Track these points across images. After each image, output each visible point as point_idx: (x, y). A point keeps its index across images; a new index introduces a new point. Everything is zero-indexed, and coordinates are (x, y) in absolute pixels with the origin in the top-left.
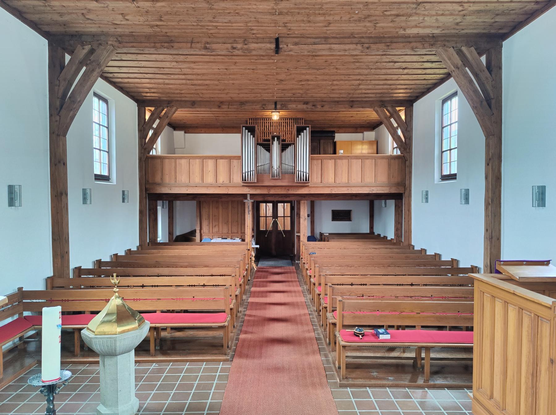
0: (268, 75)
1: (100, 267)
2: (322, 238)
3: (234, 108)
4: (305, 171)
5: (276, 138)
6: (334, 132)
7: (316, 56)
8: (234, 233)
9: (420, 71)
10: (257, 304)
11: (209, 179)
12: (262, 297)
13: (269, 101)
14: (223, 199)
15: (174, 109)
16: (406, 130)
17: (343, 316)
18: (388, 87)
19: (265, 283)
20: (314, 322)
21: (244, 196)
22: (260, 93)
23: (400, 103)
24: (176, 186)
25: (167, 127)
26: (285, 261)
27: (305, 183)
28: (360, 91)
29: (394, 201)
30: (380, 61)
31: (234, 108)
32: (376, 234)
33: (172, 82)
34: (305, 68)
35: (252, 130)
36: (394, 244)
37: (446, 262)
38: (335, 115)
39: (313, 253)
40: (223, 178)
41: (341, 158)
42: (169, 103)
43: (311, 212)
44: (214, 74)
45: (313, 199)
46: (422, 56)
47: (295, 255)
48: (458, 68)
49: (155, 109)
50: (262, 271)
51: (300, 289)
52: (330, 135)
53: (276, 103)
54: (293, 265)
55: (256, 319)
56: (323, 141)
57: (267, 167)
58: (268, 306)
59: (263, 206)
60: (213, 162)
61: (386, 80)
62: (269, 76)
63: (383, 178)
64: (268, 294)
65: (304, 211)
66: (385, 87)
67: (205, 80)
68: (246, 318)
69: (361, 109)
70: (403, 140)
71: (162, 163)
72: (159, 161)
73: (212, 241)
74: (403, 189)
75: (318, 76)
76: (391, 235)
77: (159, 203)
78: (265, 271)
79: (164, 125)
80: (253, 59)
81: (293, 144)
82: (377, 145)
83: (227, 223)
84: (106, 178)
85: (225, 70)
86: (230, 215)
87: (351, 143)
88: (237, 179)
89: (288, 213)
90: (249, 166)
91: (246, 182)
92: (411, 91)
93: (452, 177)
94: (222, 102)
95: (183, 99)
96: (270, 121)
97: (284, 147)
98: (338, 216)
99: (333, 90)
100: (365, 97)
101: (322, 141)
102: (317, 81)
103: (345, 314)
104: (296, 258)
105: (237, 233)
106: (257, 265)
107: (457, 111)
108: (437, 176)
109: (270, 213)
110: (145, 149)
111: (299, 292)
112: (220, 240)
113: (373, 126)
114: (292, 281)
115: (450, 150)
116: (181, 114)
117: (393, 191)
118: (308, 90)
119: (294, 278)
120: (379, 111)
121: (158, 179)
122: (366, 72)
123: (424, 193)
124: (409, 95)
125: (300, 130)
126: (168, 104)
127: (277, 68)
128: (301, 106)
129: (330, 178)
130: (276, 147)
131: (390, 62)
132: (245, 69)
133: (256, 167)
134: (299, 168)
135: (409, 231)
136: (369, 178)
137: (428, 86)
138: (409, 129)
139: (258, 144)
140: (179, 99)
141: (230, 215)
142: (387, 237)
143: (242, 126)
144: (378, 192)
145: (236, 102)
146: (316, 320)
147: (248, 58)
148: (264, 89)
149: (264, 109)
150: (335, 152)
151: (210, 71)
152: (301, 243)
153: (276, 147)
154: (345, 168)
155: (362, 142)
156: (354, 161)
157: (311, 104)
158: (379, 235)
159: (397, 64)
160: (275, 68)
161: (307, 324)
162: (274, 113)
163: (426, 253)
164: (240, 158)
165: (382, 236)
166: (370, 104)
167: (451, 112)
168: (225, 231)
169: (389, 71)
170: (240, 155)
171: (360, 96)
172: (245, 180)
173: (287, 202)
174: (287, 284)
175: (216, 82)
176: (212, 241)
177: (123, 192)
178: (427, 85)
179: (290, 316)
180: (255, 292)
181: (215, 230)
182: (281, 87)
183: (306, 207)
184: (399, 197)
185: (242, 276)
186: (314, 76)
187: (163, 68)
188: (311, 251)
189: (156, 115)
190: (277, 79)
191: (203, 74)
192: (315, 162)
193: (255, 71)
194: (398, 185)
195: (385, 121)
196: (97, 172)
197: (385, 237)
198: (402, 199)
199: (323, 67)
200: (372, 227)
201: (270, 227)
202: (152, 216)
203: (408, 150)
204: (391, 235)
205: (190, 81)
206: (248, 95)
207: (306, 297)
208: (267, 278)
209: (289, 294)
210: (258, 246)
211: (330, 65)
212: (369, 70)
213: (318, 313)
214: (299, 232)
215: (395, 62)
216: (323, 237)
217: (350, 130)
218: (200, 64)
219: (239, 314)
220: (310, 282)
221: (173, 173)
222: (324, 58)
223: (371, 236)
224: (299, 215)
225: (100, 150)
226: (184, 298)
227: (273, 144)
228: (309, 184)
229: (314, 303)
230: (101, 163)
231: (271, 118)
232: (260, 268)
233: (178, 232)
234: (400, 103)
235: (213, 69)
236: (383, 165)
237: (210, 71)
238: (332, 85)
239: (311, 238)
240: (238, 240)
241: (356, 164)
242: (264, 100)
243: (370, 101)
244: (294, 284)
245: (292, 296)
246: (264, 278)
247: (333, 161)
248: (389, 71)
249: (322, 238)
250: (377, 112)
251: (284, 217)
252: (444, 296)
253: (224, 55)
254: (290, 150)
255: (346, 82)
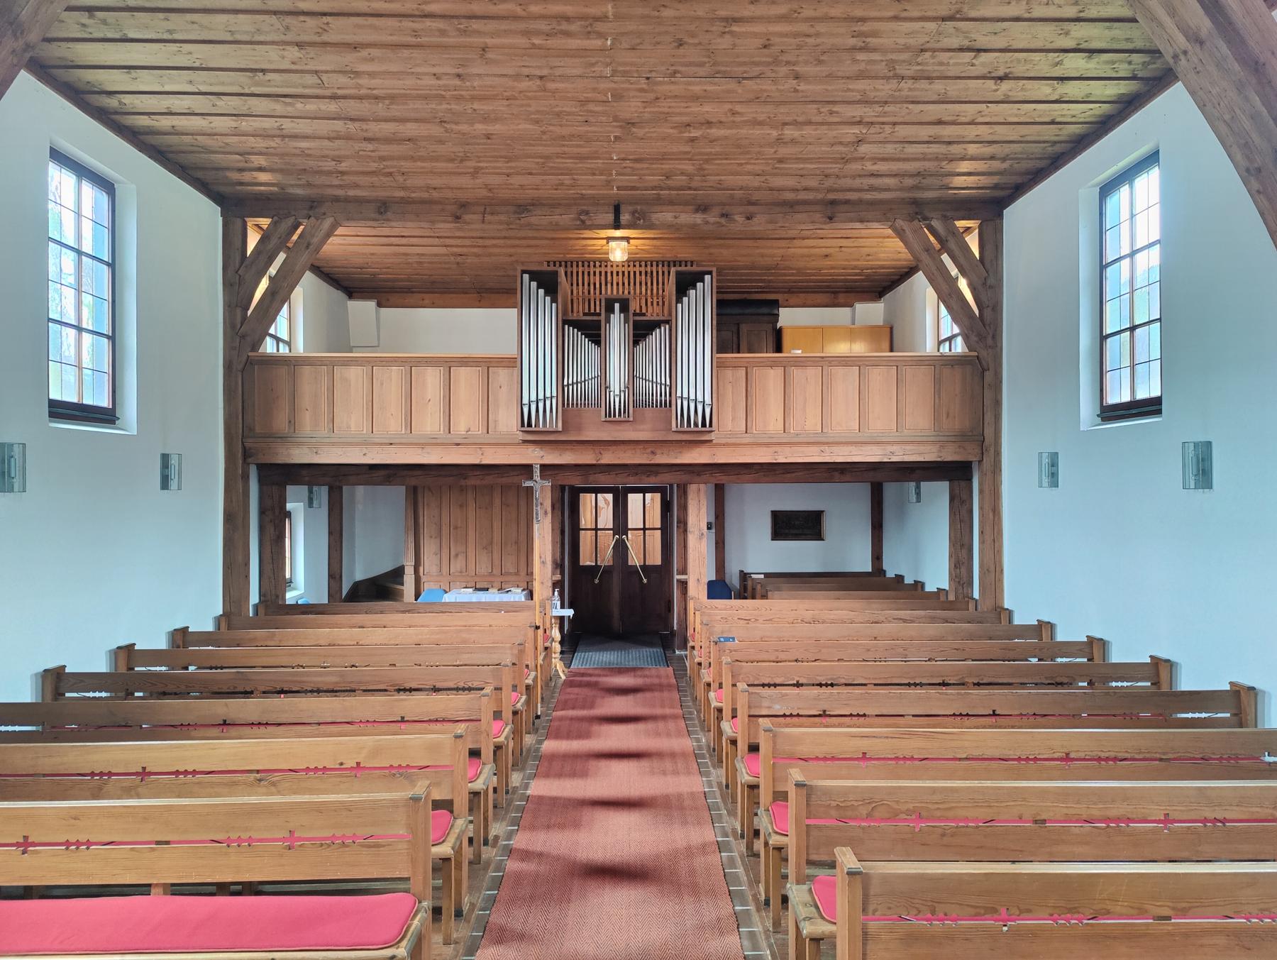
0: (588, 101)
1: (58, 694)
2: (745, 588)
3: (500, 223)
4: (700, 398)
5: (617, 306)
6: (775, 304)
7: (736, 20)
8: (508, 574)
9: (1045, 90)
10: (555, 804)
11: (429, 422)
12: (573, 775)
13: (596, 201)
14: (471, 482)
15: (328, 223)
16: (984, 284)
17: (865, 934)
18: (942, 149)
19: (585, 725)
20: (735, 879)
21: (527, 469)
22: (569, 172)
23: (966, 207)
24: (333, 444)
25: (309, 277)
26: (646, 651)
27: (700, 433)
28: (855, 167)
29: (946, 484)
30: (932, 45)
31: (500, 223)
32: (890, 574)
33: (303, 127)
34: (701, 71)
35: (548, 283)
36: (949, 606)
37: (1069, 648)
38: (781, 252)
39: (727, 639)
40: (466, 421)
41: (800, 362)
42: (313, 205)
43: (717, 517)
44: (426, 97)
45: (722, 478)
46: (1066, 25)
47: (673, 633)
48: (1201, 43)
49: (274, 224)
50: (580, 685)
51: (687, 744)
52: (765, 310)
53: (617, 211)
54: (667, 662)
55: (543, 868)
56: (747, 320)
57: (592, 386)
58: (587, 813)
59: (587, 500)
60: (450, 381)
61: (940, 122)
62: (591, 107)
63: (919, 419)
64: (593, 764)
65: (698, 514)
66: (934, 149)
67: (403, 120)
68: (512, 865)
69: (858, 225)
70: (977, 312)
71: (294, 378)
72: (283, 371)
73: (448, 598)
74: (978, 450)
75: (738, 108)
76: (937, 577)
77: (291, 490)
78: (588, 685)
79: (297, 268)
80: (538, 33)
81: (667, 322)
82: (889, 335)
83: (488, 547)
84: (105, 416)
85: (457, 82)
86: (497, 524)
87: (823, 333)
88: (507, 422)
89: (655, 519)
90: (539, 384)
91: (530, 430)
92: (1006, 165)
93: (1151, 407)
94: (464, 205)
95: (351, 193)
96: (603, 270)
97: (641, 331)
98: (792, 526)
99: (781, 161)
100: (872, 188)
101: (744, 328)
102: (734, 125)
103: (873, 926)
104: (677, 641)
105: (517, 574)
106: (568, 665)
107: (1155, 213)
108: (1087, 408)
109: (606, 519)
110: (243, 337)
111: (684, 755)
112: (468, 595)
113: (882, 284)
114: (664, 718)
115: (1133, 329)
116: (347, 242)
117: (949, 455)
118: (707, 161)
119: (672, 707)
120: (909, 233)
121: (280, 422)
122: (885, 89)
123: (1046, 461)
124: (995, 180)
125: (685, 284)
126: (311, 208)
127: (614, 72)
128: (688, 217)
129: (770, 420)
130: (616, 329)
131: (961, 50)
132: (517, 77)
133: (562, 387)
134: (683, 389)
135: (994, 572)
136: (882, 419)
137: (1058, 148)
138: (991, 281)
139: (565, 322)
140: (340, 192)
141: (497, 524)
142: (923, 585)
143: (519, 268)
144: (907, 459)
145: (505, 202)
146: (740, 870)
147: (522, 26)
148: (581, 158)
149: (584, 226)
150: (779, 349)
151: (410, 82)
152: (691, 605)
153: (616, 329)
154: (813, 390)
155: (852, 333)
156: (839, 371)
157: (716, 211)
158: (900, 578)
159: (984, 57)
160: (608, 71)
161: (713, 893)
162: (613, 244)
163: (1052, 636)
164: (514, 363)
165: (909, 580)
166: (881, 210)
167: (1132, 216)
168: (484, 568)
169: (954, 89)
170: (514, 352)
171: (858, 183)
172: (529, 425)
173: (652, 490)
174: (650, 726)
175: (436, 130)
176: (448, 598)
177: (165, 458)
178: (1055, 142)
179: (658, 856)
180: (553, 757)
181: (457, 565)
182: (629, 147)
183: (704, 502)
184: (962, 472)
185: (507, 715)
186: (728, 106)
187: (263, 71)
188: (718, 628)
189: (274, 241)
190: (616, 119)
191: (392, 98)
192: (729, 373)
193: (551, 86)
194: (962, 438)
195: (925, 257)
196: (62, 389)
197: (919, 585)
198: (970, 480)
199: (756, 70)
200: (877, 557)
201: (607, 558)
202: (270, 530)
203: (990, 341)
204: (937, 577)
205: (357, 124)
206: (536, 180)
207: (708, 774)
208: (592, 707)
209: (655, 763)
210: (569, 612)
211: (776, 62)
212: (893, 84)
213: (750, 846)
214: (684, 571)
215: (979, 51)
216: (749, 583)
217: (820, 298)
218: (375, 52)
219: (488, 853)
220: (720, 733)
221: (324, 406)
222: (758, 28)
223: (876, 582)
224: (685, 524)
225: (80, 329)
226: (255, 835)
227: (608, 321)
228: (712, 436)
229: (734, 801)
230: (80, 367)
231: (607, 260)
232: (576, 674)
233: (359, 570)
234: (966, 207)
235: (418, 76)
236: (919, 383)
237: (410, 82)
238: (780, 141)
239: (718, 589)
240: (517, 595)
241: (845, 381)
242: (583, 197)
243: (882, 202)
244: (671, 725)
245: (664, 773)
246: (583, 708)
247: (780, 371)
248: (954, 89)
249: (747, 588)
250: (900, 234)
251: (644, 529)
252: (1211, 816)
253: (443, 17)
254: (657, 338)
255: (823, 130)
